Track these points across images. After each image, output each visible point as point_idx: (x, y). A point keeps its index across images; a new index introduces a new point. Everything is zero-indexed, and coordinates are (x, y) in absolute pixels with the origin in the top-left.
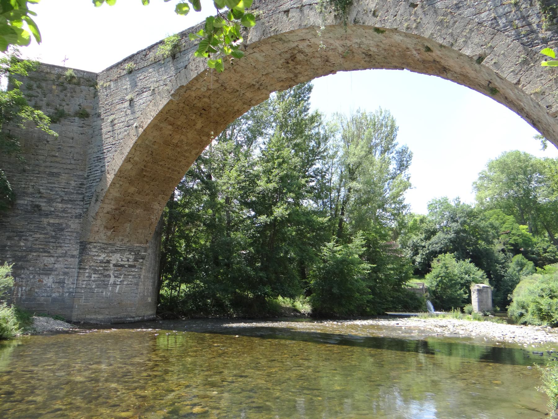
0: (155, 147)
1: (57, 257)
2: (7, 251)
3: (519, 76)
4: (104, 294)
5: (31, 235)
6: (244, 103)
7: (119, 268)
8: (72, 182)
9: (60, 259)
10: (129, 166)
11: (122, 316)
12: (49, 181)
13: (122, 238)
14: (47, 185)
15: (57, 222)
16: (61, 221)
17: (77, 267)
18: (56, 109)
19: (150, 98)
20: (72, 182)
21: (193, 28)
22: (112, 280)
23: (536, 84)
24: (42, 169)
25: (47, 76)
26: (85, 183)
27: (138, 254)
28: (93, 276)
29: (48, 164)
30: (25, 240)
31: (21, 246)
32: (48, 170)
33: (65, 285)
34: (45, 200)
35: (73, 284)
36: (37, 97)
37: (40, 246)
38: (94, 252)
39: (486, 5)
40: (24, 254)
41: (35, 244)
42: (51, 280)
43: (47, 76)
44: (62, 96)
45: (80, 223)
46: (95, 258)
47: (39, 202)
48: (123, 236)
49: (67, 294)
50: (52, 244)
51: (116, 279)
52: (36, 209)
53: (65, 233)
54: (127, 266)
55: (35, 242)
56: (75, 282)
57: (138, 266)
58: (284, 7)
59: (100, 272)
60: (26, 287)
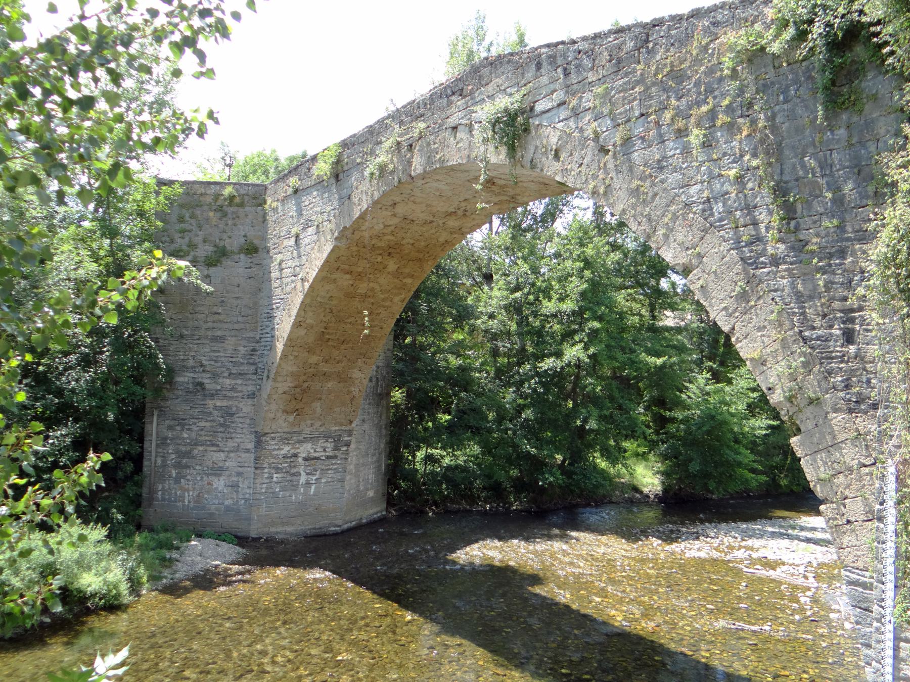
0: (334, 302)
2: (170, 444)
3: (733, 320)
7: (312, 462)
8: (241, 348)
9: (232, 455)
10: (302, 332)
15: (225, 404)
16: (230, 403)
17: (252, 465)
19: (315, 237)
20: (241, 348)
21: (355, 135)
22: (303, 479)
23: (755, 342)
24: (202, 332)
25: (201, 199)
28: (275, 476)
29: (210, 325)
30: (188, 429)
31: (184, 438)
32: (209, 333)
35: (249, 487)
36: (190, 231)
37: (207, 438)
38: (272, 445)
39: (698, 172)
40: (189, 448)
42: (222, 483)
43: (201, 199)
44: (222, 226)
48: (312, 419)
51: (310, 477)
52: (199, 388)
58: (452, 121)
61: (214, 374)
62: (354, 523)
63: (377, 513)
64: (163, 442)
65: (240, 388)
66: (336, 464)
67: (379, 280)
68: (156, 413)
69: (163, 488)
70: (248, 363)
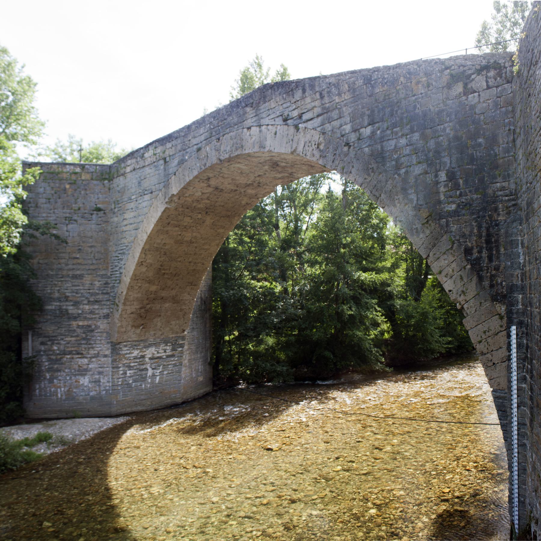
2: (42, 355)
4: (143, 386)
5: (62, 339)
7: (156, 360)
8: (96, 283)
9: (94, 360)
12: (74, 284)
14: (72, 288)
16: (90, 322)
20: (96, 283)
22: (150, 372)
24: (65, 273)
26: (109, 282)
27: (175, 343)
28: (128, 372)
29: (71, 267)
31: (54, 350)
32: (71, 273)
34: (72, 303)
35: (108, 382)
37: (73, 349)
38: (125, 351)
40: (59, 357)
41: (68, 347)
45: (109, 323)
47: (67, 305)
48: (154, 330)
49: (104, 392)
50: (83, 346)
51: (155, 371)
53: (95, 334)
54: (165, 357)
56: (111, 380)
59: (135, 368)
65: (97, 312)
66: (174, 360)
70: (102, 293)
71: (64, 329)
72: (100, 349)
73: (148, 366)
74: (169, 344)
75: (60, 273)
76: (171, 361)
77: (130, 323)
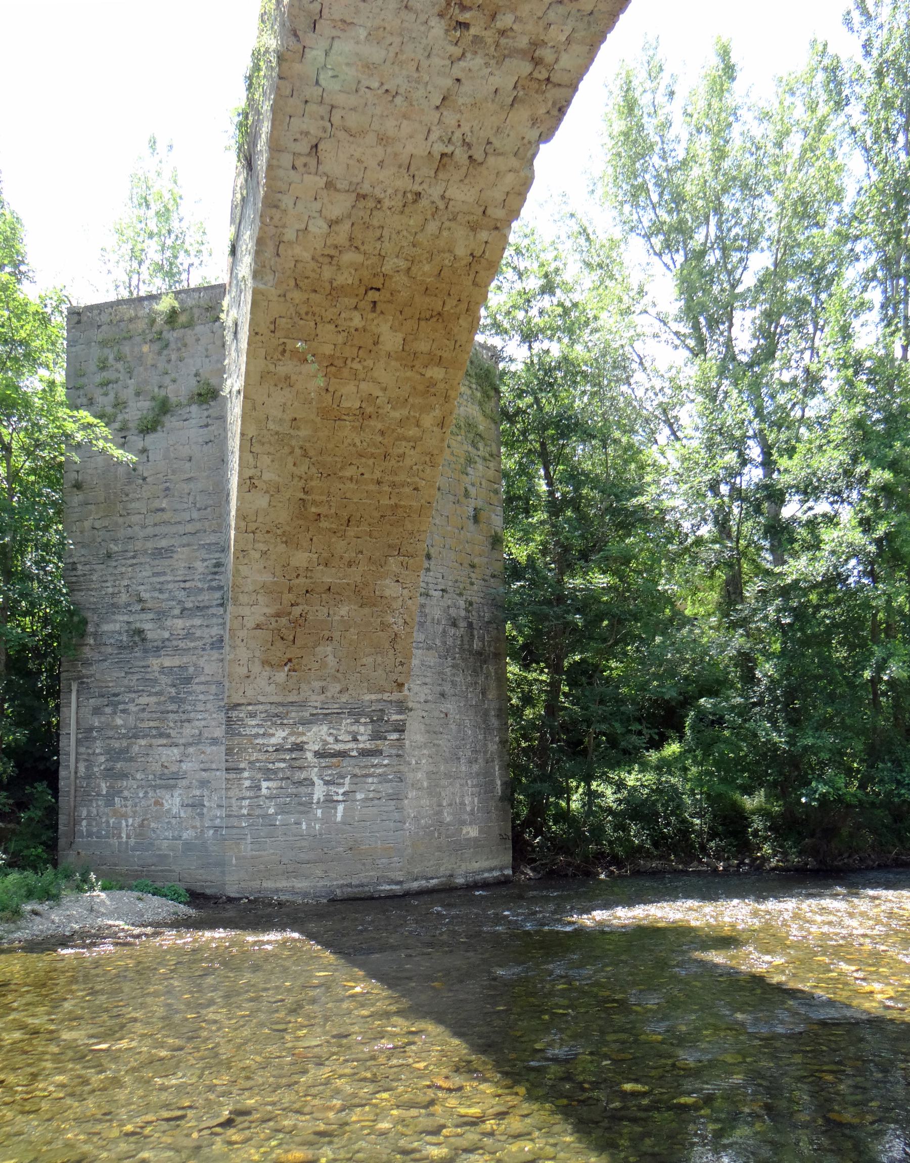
0: (304, 433)
1: (185, 745)
4: (304, 827)
6: (474, 228)
7: (334, 760)
9: (191, 750)
11: (365, 881)
13: (324, 683)
18: (153, 399)
22: (319, 791)
24: (139, 545)
25: (131, 327)
28: (264, 784)
29: (150, 531)
30: (124, 711)
31: (117, 727)
32: (150, 545)
33: (205, 810)
34: (151, 616)
35: (220, 806)
37: (152, 724)
38: (252, 726)
40: (125, 743)
42: (177, 800)
43: (131, 327)
46: (260, 741)
49: (211, 832)
50: (171, 716)
51: (333, 788)
52: (136, 638)
54: (354, 753)
55: (142, 715)
57: (387, 751)
60: (134, 817)
61: (158, 613)
62: (434, 882)
63: (491, 870)
64: (86, 735)
65: (198, 633)
67: (376, 374)
68: (74, 687)
69: (89, 812)
70: (211, 588)
71: (135, 677)
72: (203, 723)
73: (314, 774)
74: (363, 720)
75: (131, 547)
76: (373, 766)
77: (257, 654)
